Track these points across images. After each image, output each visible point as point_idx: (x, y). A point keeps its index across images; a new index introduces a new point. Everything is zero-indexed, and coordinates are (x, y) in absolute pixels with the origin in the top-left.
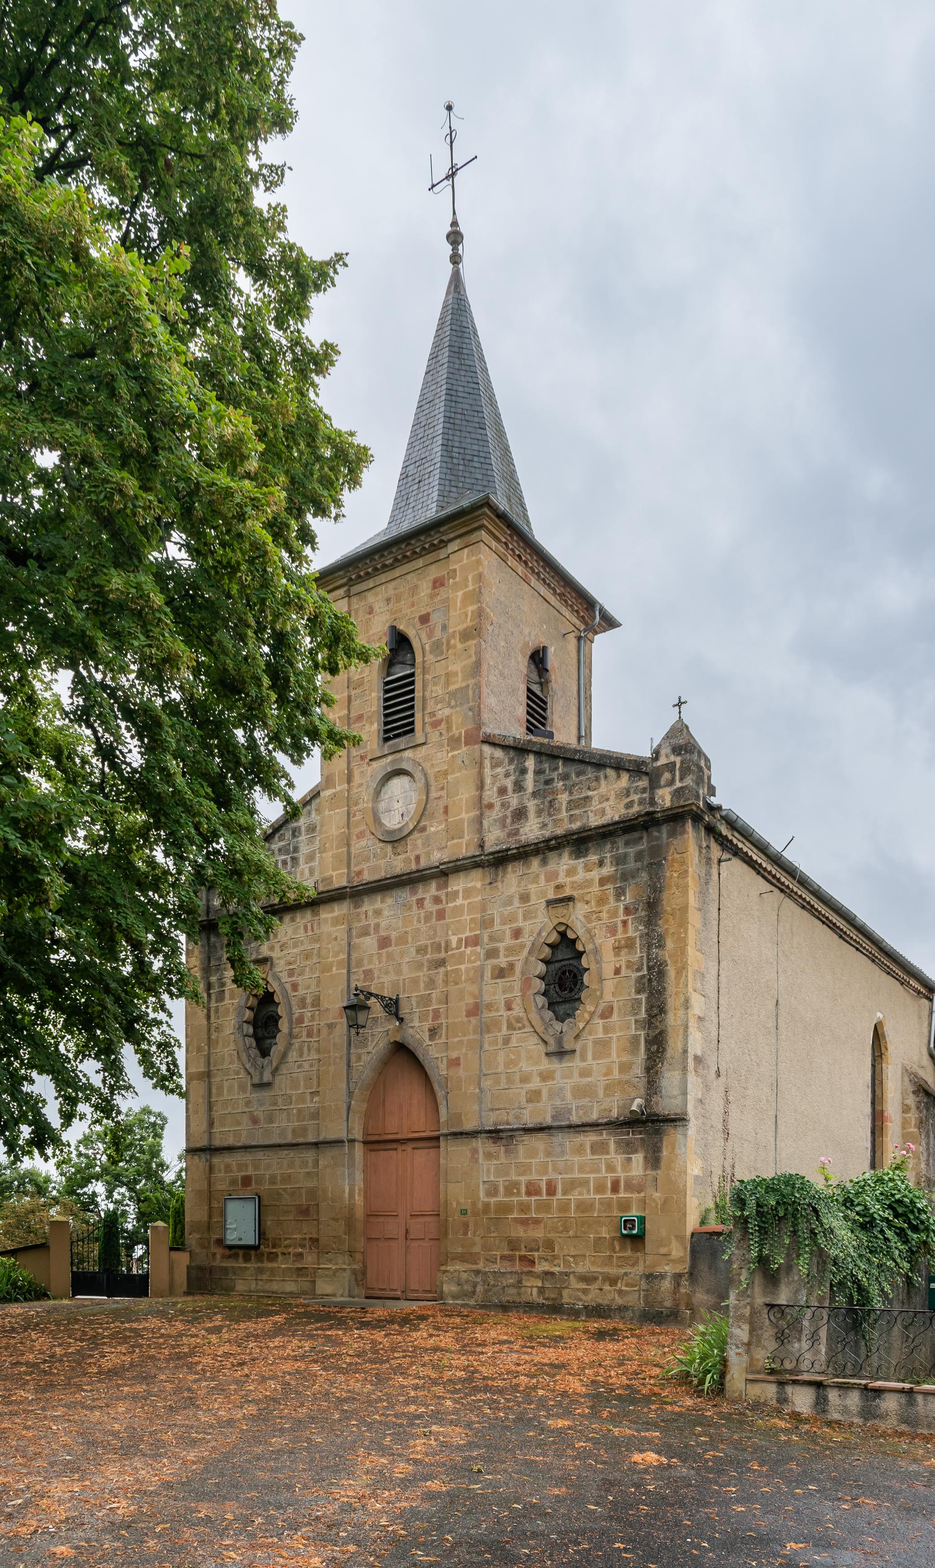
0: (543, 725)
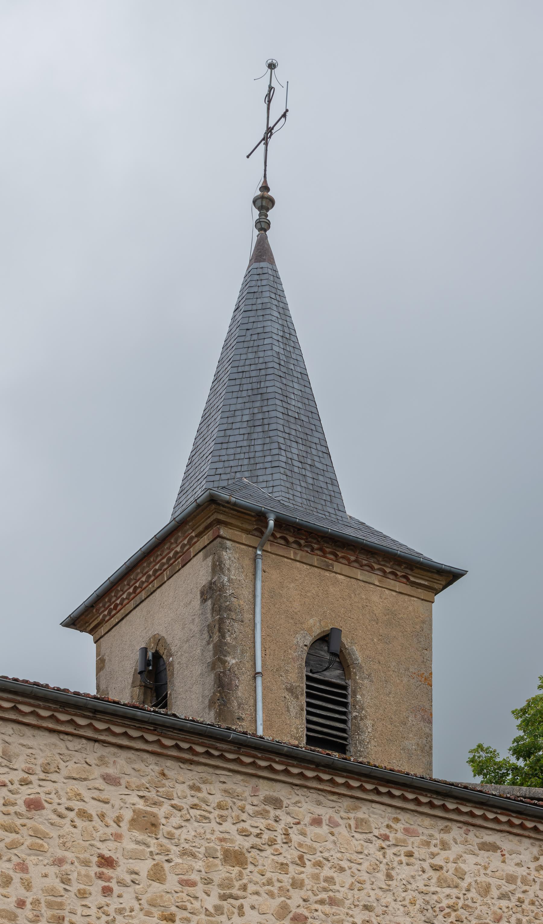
0: (344, 722)
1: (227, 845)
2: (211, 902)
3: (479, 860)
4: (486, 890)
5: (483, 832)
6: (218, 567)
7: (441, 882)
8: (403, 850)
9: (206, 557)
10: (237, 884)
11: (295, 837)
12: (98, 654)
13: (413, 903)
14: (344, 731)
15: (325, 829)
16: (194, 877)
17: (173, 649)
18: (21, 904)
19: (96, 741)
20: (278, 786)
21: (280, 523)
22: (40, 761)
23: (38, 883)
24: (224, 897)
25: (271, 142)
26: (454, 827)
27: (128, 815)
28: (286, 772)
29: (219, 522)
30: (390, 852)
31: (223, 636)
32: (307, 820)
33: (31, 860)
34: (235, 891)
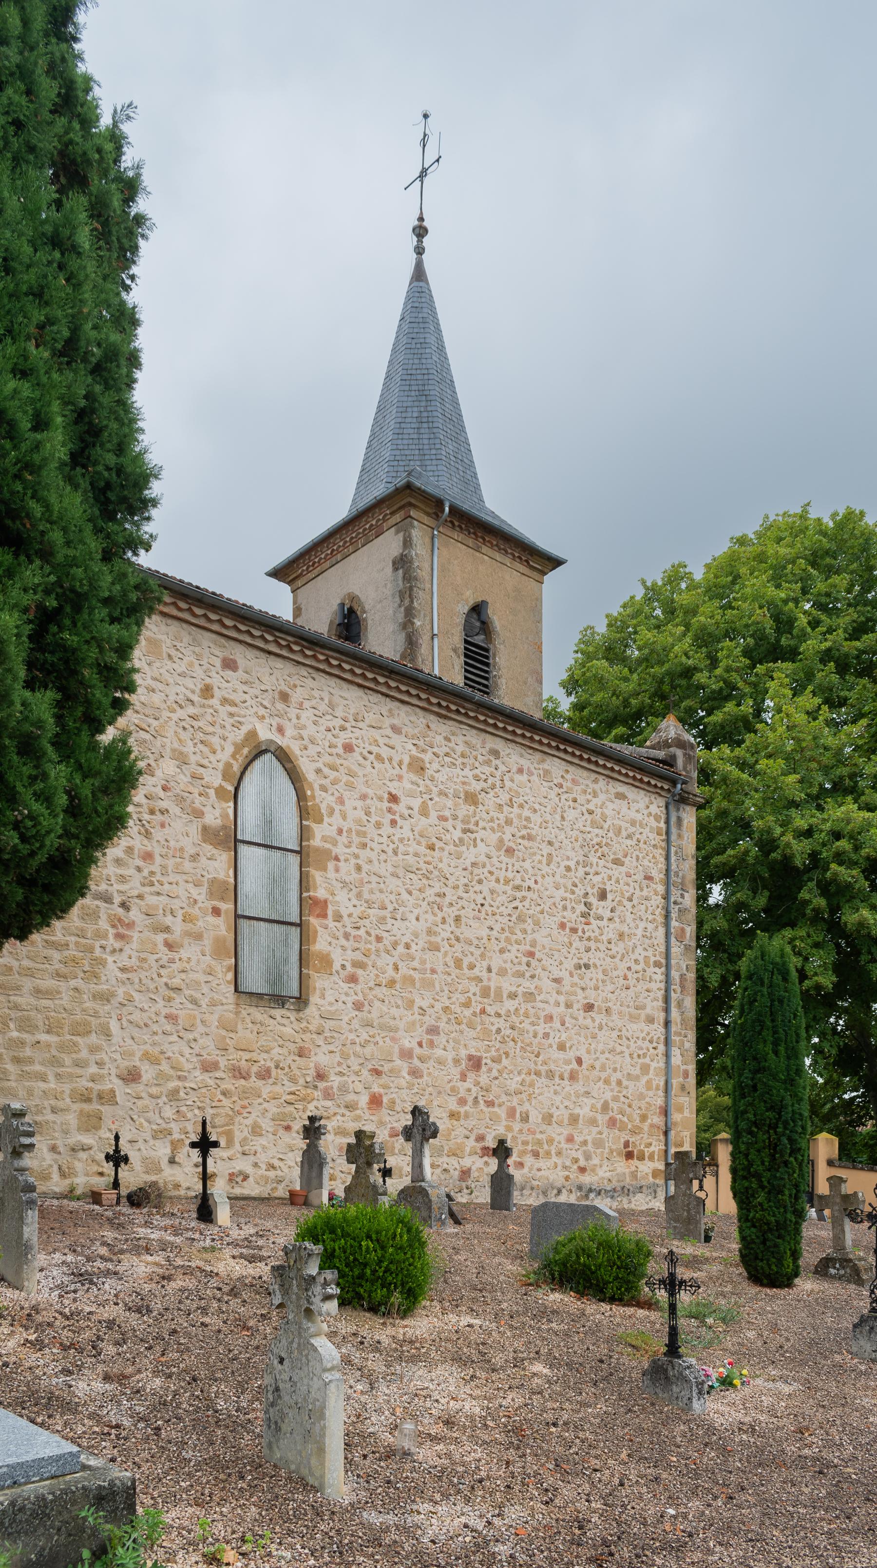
0: (487, 679)
1: (467, 788)
2: (457, 834)
4: (618, 832)
5: (618, 784)
6: (407, 543)
7: (594, 824)
8: (571, 796)
9: (397, 532)
10: (473, 820)
11: (508, 783)
12: (295, 602)
14: (486, 686)
15: (524, 778)
16: (447, 813)
17: (367, 607)
18: (340, 832)
19: (387, 696)
20: (498, 740)
21: (456, 511)
22: (352, 711)
23: (351, 814)
24: (465, 831)
25: (426, 180)
26: (601, 778)
27: (406, 760)
28: (505, 729)
29: (410, 505)
30: (563, 797)
31: (412, 602)
32: (514, 769)
33: (346, 795)
34: (471, 826)
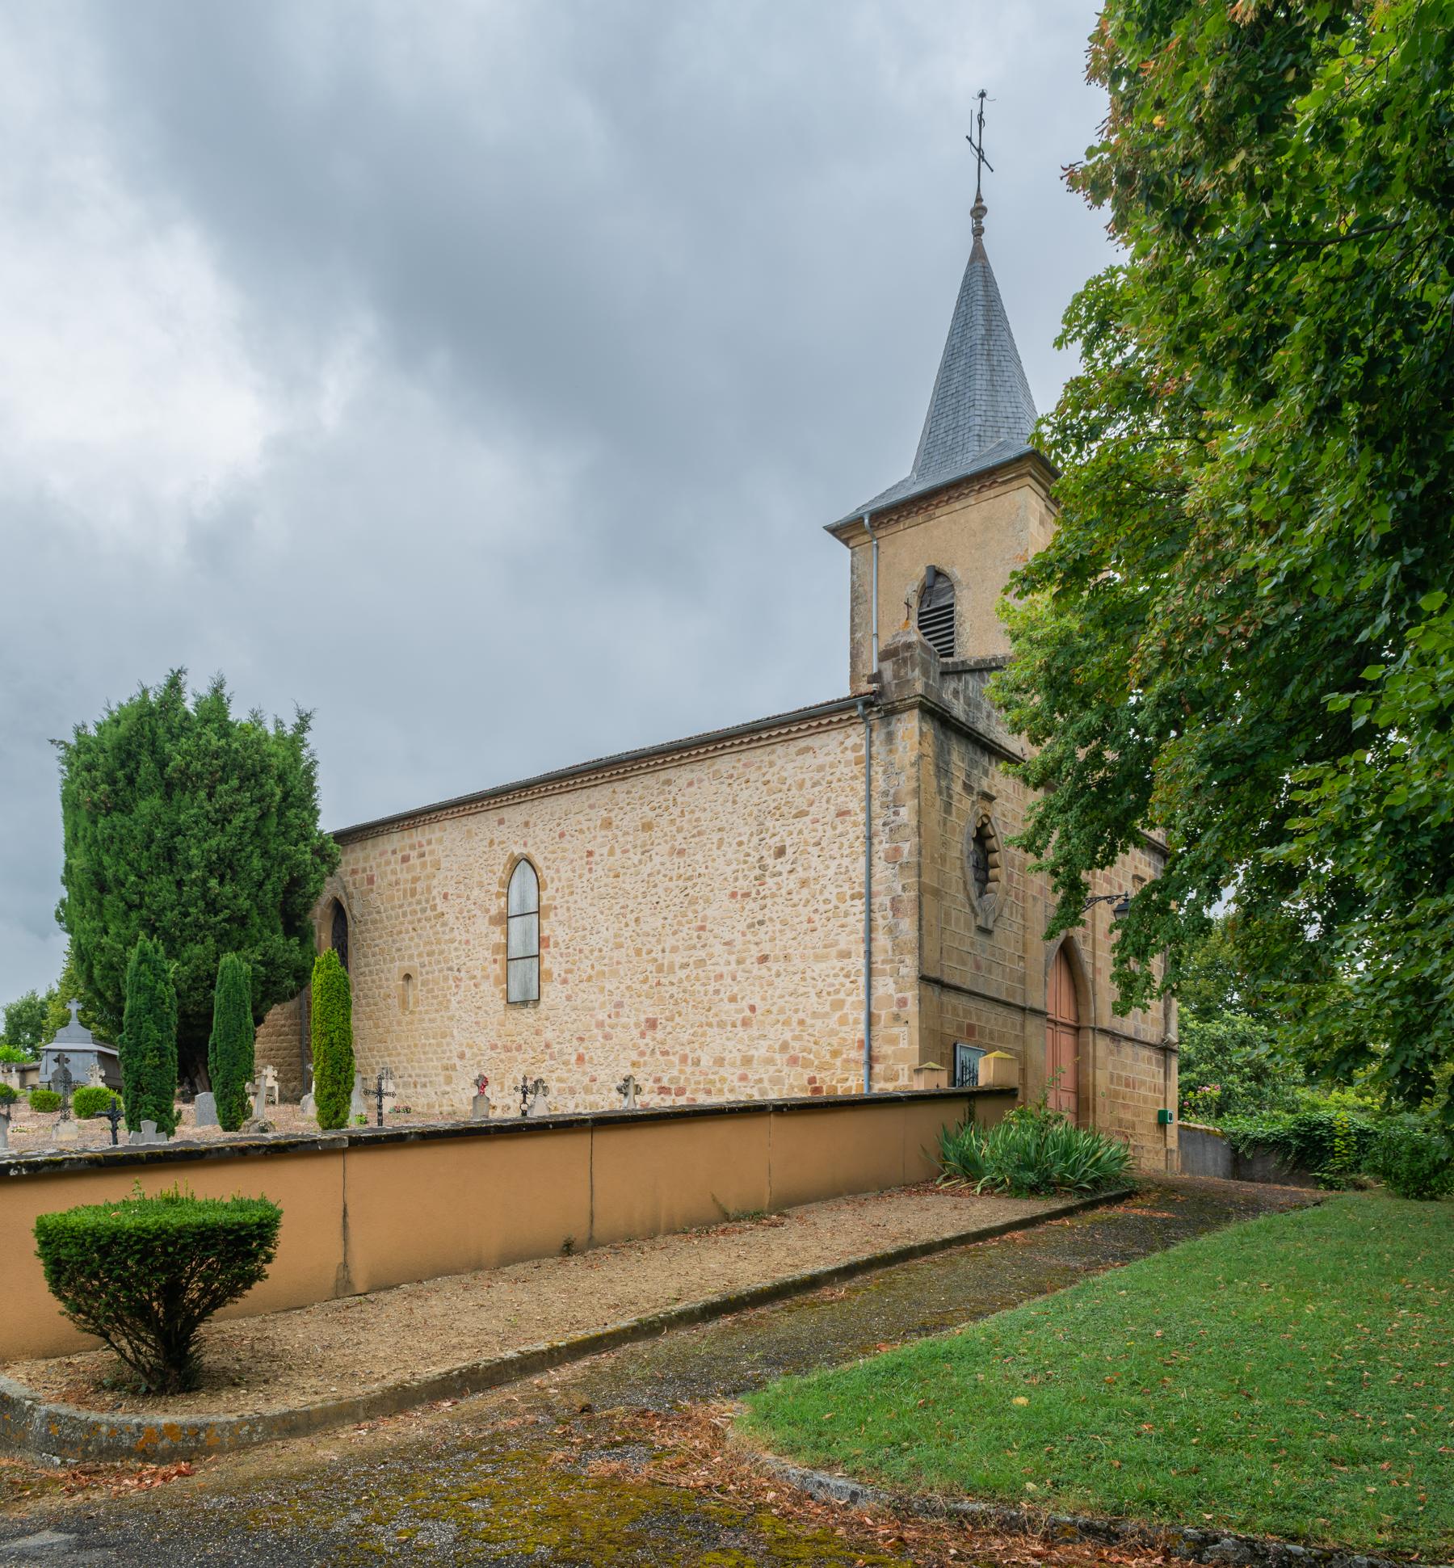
3: (797, 764)
7: (770, 792)
13: (750, 815)
16: (629, 846)
26: (778, 746)
